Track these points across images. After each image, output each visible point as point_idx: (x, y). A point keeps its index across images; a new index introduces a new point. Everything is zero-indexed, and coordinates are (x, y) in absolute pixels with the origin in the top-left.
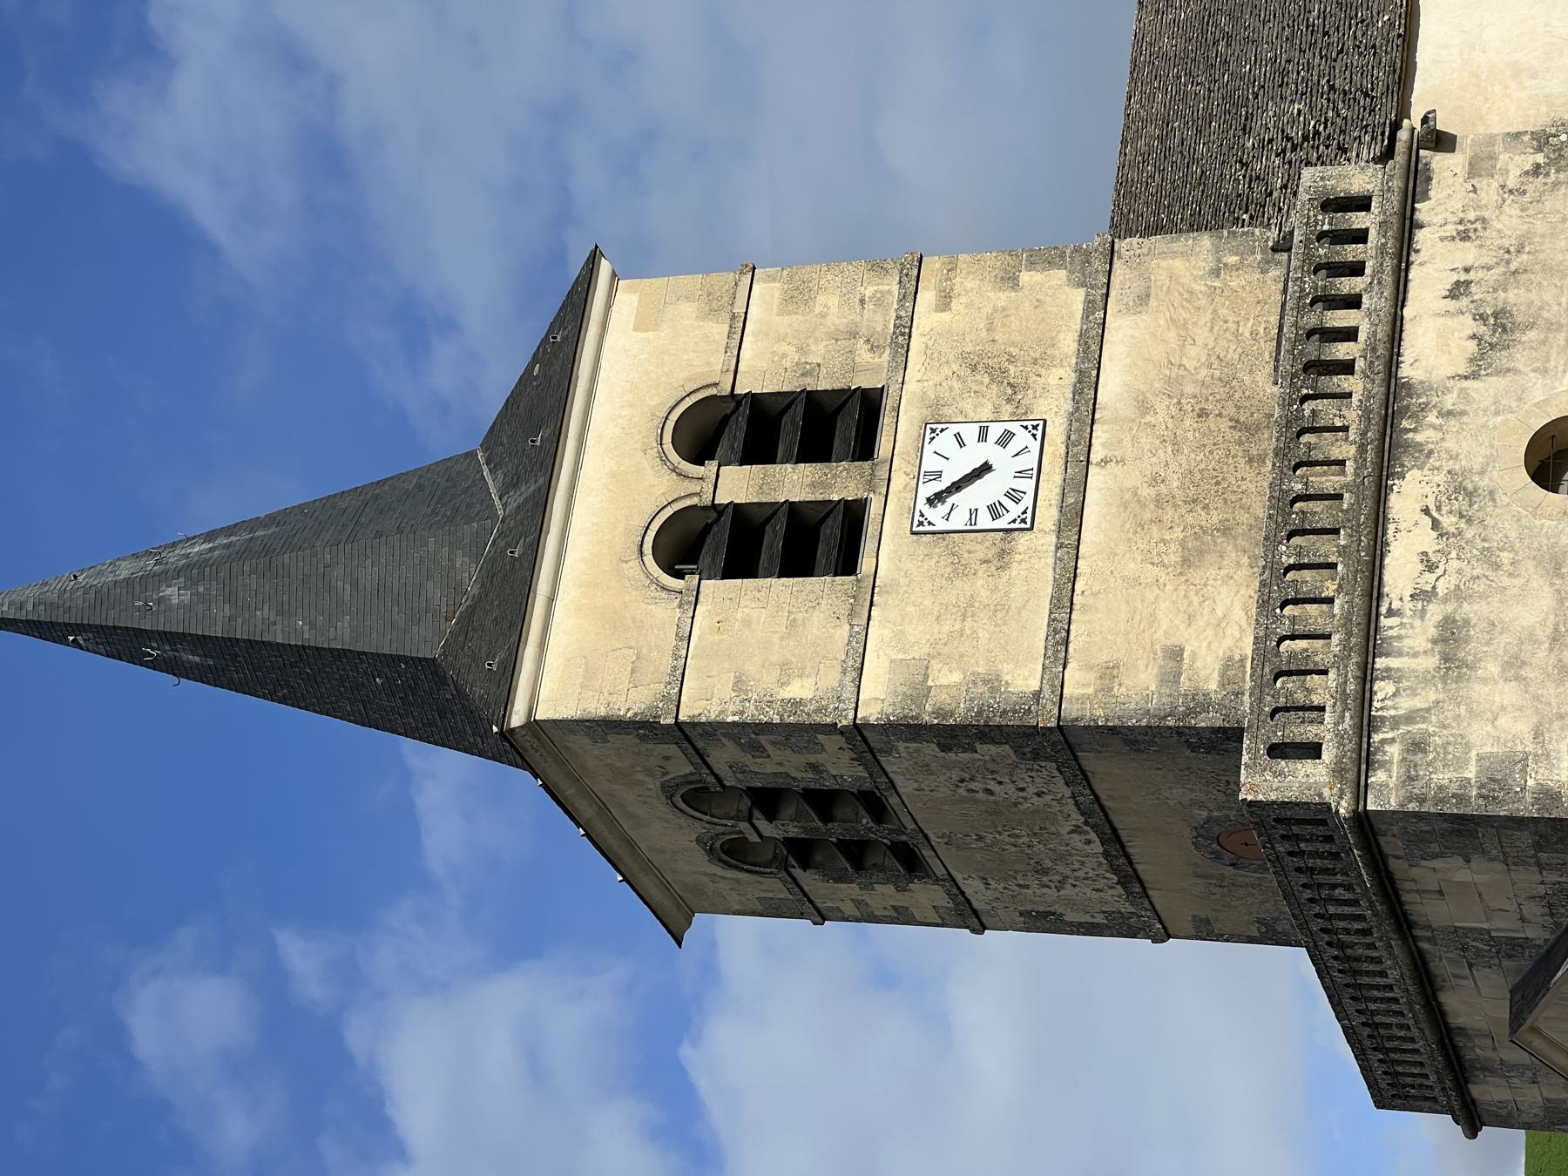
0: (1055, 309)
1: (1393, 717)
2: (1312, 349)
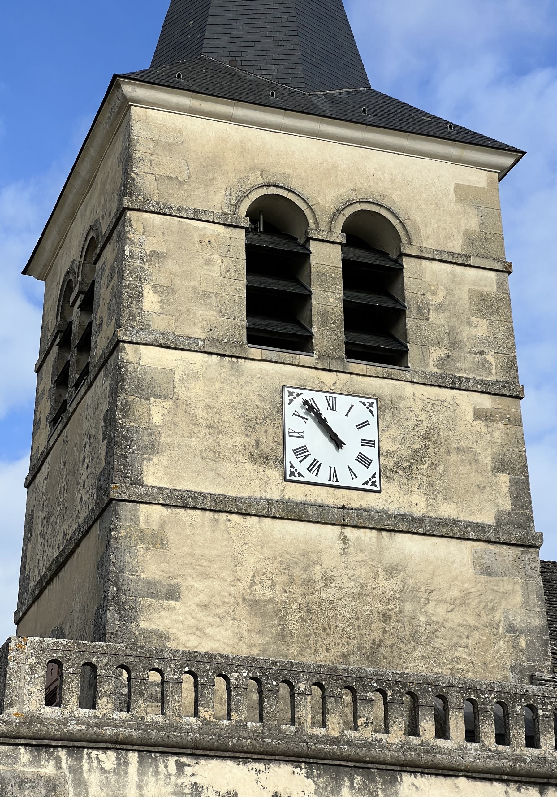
0: (476, 501)
1: (81, 768)
2: (428, 698)
